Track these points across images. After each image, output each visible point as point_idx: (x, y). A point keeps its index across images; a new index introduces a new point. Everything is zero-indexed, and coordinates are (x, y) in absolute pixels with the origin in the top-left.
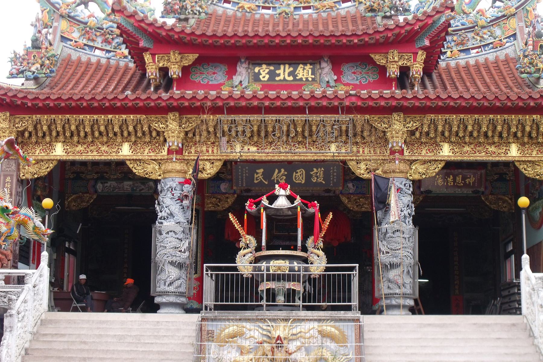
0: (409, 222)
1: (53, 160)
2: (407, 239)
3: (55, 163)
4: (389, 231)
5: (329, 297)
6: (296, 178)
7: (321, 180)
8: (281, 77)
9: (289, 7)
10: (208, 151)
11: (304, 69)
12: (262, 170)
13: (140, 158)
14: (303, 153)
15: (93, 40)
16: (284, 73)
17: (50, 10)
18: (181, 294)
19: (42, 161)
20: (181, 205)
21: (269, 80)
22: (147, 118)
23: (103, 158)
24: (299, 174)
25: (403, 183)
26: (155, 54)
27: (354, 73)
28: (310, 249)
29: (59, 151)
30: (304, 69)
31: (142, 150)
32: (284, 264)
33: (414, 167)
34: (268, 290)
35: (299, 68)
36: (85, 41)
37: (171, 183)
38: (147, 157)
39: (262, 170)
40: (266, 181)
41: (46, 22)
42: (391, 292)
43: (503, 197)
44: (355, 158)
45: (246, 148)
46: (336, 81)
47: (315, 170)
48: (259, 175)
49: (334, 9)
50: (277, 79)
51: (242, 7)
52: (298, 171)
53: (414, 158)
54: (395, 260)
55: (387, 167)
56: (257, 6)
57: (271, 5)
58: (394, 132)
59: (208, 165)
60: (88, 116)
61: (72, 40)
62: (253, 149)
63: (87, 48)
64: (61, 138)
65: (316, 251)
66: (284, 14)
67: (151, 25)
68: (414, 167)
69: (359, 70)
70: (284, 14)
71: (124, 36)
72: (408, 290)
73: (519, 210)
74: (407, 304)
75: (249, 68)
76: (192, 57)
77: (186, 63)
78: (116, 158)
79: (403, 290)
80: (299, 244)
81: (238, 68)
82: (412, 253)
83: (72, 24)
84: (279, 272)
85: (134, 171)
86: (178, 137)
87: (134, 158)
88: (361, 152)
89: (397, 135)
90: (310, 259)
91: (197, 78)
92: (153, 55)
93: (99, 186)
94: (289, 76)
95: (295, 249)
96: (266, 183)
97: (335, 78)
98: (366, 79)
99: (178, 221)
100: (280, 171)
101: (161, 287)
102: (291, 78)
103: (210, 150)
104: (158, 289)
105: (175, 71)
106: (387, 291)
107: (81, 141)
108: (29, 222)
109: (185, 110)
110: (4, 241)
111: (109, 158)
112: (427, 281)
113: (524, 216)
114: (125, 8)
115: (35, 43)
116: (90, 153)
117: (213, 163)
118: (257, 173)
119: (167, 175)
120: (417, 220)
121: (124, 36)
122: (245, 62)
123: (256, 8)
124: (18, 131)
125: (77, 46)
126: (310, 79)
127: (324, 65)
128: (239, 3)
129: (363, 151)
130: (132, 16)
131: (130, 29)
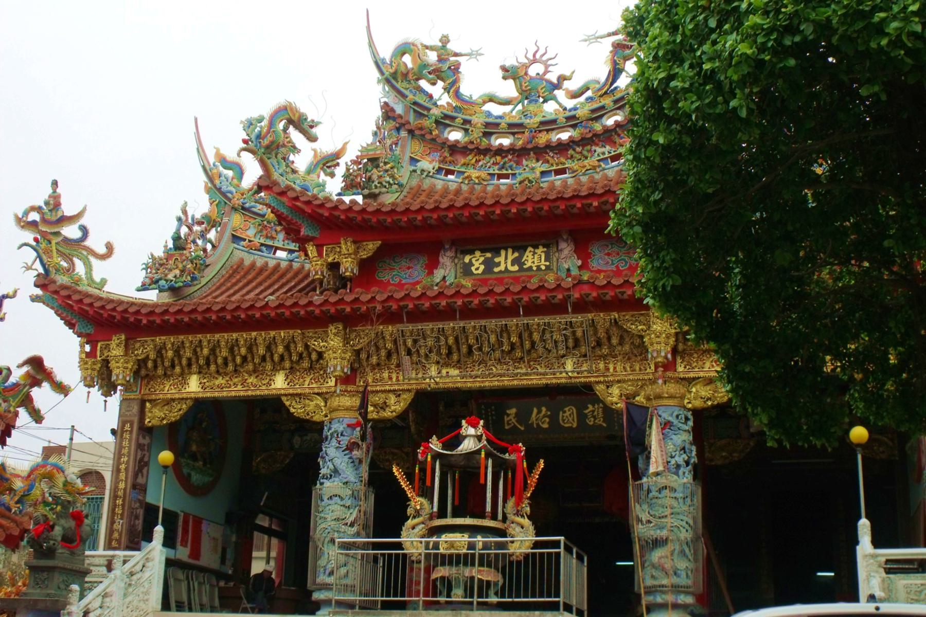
0: (684, 473)
1: (187, 399)
2: (681, 501)
3: (190, 403)
4: (653, 489)
5: (526, 590)
6: (563, 420)
7: (600, 421)
8: (502, 267)
9: (534, 172)
10: (390, 378)
11: (534, 253)
12: (513, 411)
13: (299, 391)
14: (526, 374)
15: (273, 238)
16: (505, 262)
17: (219, 202)
18: (351, 589)
19: (173, 400)
20: (350, 458)
21: (484, 272)
22: (303, 334)
23: (250, 393)
24: (568, 413)
25: (675, 414)
26: (322, 246)
27: (608, 254)
28: (511, 517)
29: (194, 386)
30: (534, 253)
31: (301, 380)
32: (461, 539)
33: (694, 390)
34: (443, 578)
35: (527, 253)
36: (262, 241)
37: (338, 427)
38: (307, 391)
39: (513, 411)
40: (521, 425)
41: (214, 217)
42: (656, 583)
43: (880, 437)
44: (602, 379)
45: (444, 372)
46: (580, 268)
47: (590, 407)
48: (511, 417)
49: (598, 170)
50: (496, 270)
51: (469, 177)
52: (567, 409)
53: (692, 375)
54: (664, 533)
55: (649, 390)
56: (489, 174)
57: (510, 171)
58: (653, 336)
59: (392, 399)
60: (226, 335)
61: (245, 240)
62: (454, 372)
63: (264, 249)
64: (194, 368)
65: (519, 519)
66: (526, 182)
67: (308, 203)
68: (694, 390)
69: (616, 249)
70: (526, 182)
71: (284, 223)
72: (683, 580)
73: (850, 448)
74: (680, 602)
75: (456, 257)
76: (371, 247)
77: (364, 255)
78: (266, 392)
79: (675, 580)
80: (488, 508)
81: (441, 259)
82: (691, 522)
83: (247, 218)
84: (453, 551)
85: (292, 410)
86: (343, 359)
87: (291, 391)
88: (611, 370)
89: (658, 340)
90: (510, 531)
91: (384, 276)
92: (319, 248)
93: (297, 440)
94: (513, 265)
95: (482, 515)
96: (522, 429)
97: (580, 263)
98: (626, 262)
99: (345, 480)
100: (539, 412)
101: (322, 578)
102: (516, 268)
103: (394, 376)
104: (318, 580)
105: (348, 267)
106: (649, 582)
107: (221, 371)
108: (58, 475)
109: (351, 320)
110: (17, 503)
111: (258, 393)
112: (833, 574)
113: (859, 457)
114: (276, 183)
115: (177, 243)
116: (233, 388)
117: (399, 395)
118: (508, 415)
119: (334, 415)
120: (701, 472)
121: (284, 223)
122: (450, 249)
123: (489, 177)
124: (138, 360)
125: (252, 248)
126: (543, 268)
127: (563, 245)
128: (464, 173)
129: (615, 368)
130: (282, 193)
131: (283, 210)
